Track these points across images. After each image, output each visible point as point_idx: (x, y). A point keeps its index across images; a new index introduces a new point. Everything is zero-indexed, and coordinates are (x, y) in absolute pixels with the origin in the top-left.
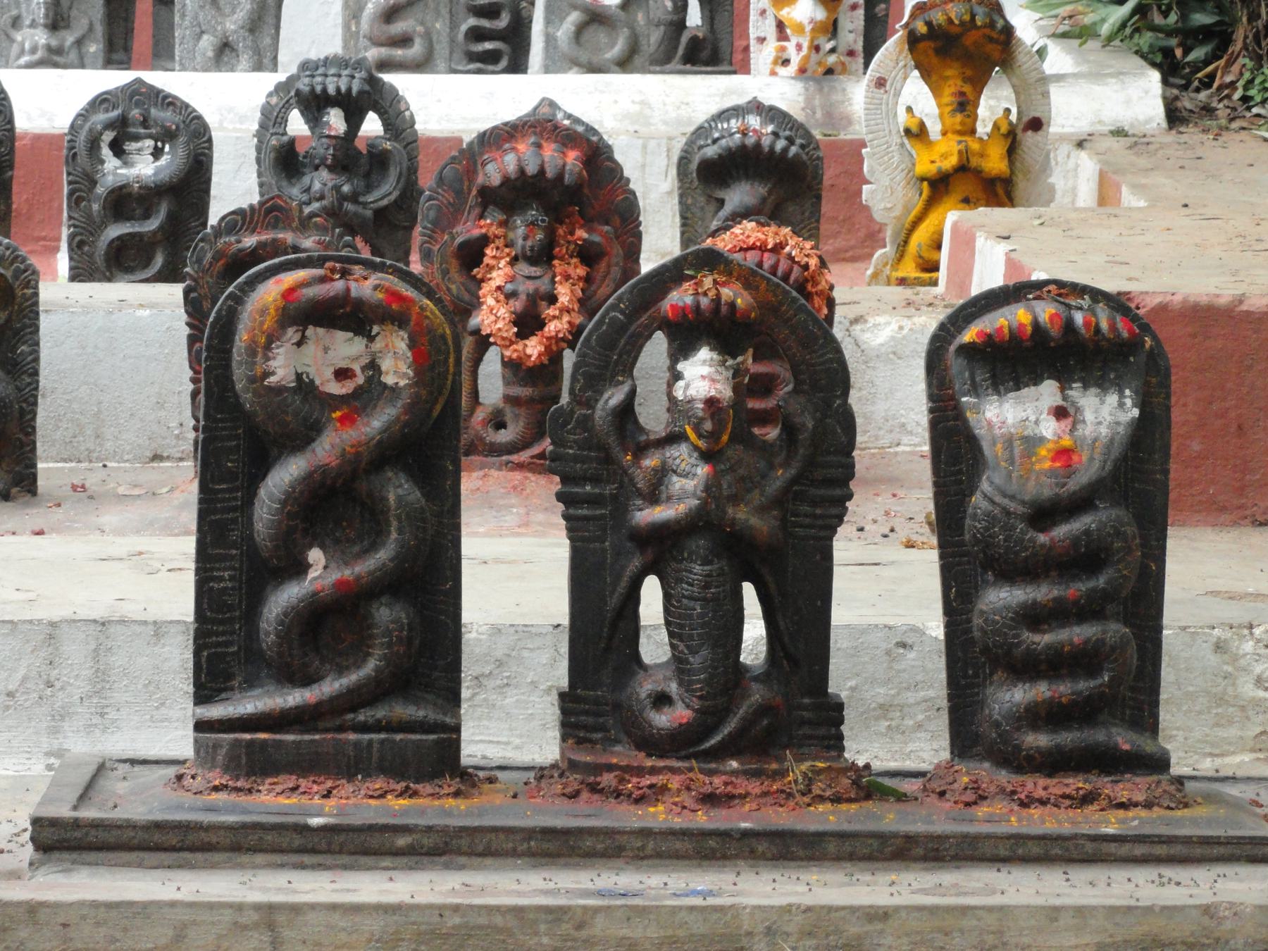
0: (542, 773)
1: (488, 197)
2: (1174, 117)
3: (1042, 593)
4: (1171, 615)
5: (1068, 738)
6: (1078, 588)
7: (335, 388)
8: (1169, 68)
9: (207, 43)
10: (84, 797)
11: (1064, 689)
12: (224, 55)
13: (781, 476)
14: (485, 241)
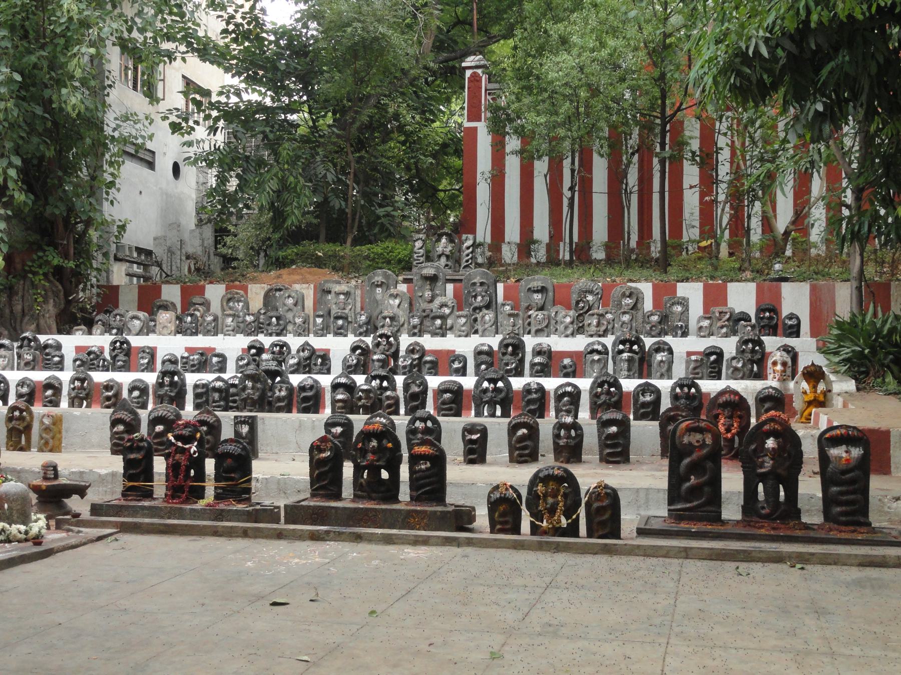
0: (738, 522)
1: (720, 405)
2: (858, 389)
3: (844, 488)
4: (871, 493)
5: (850, 518)
6: (851, 488)
7: (696, 444)
8: (856, 379)
9: (658, 374)
10: (646, 524)
11: (848, 508)
12: (662, 377)
13: (787, 464)
14: (719, 414)
